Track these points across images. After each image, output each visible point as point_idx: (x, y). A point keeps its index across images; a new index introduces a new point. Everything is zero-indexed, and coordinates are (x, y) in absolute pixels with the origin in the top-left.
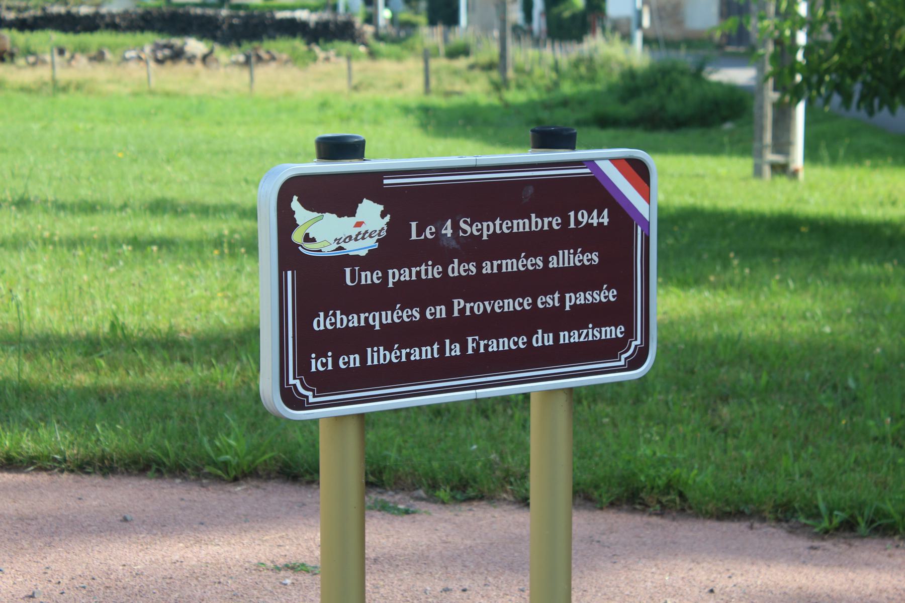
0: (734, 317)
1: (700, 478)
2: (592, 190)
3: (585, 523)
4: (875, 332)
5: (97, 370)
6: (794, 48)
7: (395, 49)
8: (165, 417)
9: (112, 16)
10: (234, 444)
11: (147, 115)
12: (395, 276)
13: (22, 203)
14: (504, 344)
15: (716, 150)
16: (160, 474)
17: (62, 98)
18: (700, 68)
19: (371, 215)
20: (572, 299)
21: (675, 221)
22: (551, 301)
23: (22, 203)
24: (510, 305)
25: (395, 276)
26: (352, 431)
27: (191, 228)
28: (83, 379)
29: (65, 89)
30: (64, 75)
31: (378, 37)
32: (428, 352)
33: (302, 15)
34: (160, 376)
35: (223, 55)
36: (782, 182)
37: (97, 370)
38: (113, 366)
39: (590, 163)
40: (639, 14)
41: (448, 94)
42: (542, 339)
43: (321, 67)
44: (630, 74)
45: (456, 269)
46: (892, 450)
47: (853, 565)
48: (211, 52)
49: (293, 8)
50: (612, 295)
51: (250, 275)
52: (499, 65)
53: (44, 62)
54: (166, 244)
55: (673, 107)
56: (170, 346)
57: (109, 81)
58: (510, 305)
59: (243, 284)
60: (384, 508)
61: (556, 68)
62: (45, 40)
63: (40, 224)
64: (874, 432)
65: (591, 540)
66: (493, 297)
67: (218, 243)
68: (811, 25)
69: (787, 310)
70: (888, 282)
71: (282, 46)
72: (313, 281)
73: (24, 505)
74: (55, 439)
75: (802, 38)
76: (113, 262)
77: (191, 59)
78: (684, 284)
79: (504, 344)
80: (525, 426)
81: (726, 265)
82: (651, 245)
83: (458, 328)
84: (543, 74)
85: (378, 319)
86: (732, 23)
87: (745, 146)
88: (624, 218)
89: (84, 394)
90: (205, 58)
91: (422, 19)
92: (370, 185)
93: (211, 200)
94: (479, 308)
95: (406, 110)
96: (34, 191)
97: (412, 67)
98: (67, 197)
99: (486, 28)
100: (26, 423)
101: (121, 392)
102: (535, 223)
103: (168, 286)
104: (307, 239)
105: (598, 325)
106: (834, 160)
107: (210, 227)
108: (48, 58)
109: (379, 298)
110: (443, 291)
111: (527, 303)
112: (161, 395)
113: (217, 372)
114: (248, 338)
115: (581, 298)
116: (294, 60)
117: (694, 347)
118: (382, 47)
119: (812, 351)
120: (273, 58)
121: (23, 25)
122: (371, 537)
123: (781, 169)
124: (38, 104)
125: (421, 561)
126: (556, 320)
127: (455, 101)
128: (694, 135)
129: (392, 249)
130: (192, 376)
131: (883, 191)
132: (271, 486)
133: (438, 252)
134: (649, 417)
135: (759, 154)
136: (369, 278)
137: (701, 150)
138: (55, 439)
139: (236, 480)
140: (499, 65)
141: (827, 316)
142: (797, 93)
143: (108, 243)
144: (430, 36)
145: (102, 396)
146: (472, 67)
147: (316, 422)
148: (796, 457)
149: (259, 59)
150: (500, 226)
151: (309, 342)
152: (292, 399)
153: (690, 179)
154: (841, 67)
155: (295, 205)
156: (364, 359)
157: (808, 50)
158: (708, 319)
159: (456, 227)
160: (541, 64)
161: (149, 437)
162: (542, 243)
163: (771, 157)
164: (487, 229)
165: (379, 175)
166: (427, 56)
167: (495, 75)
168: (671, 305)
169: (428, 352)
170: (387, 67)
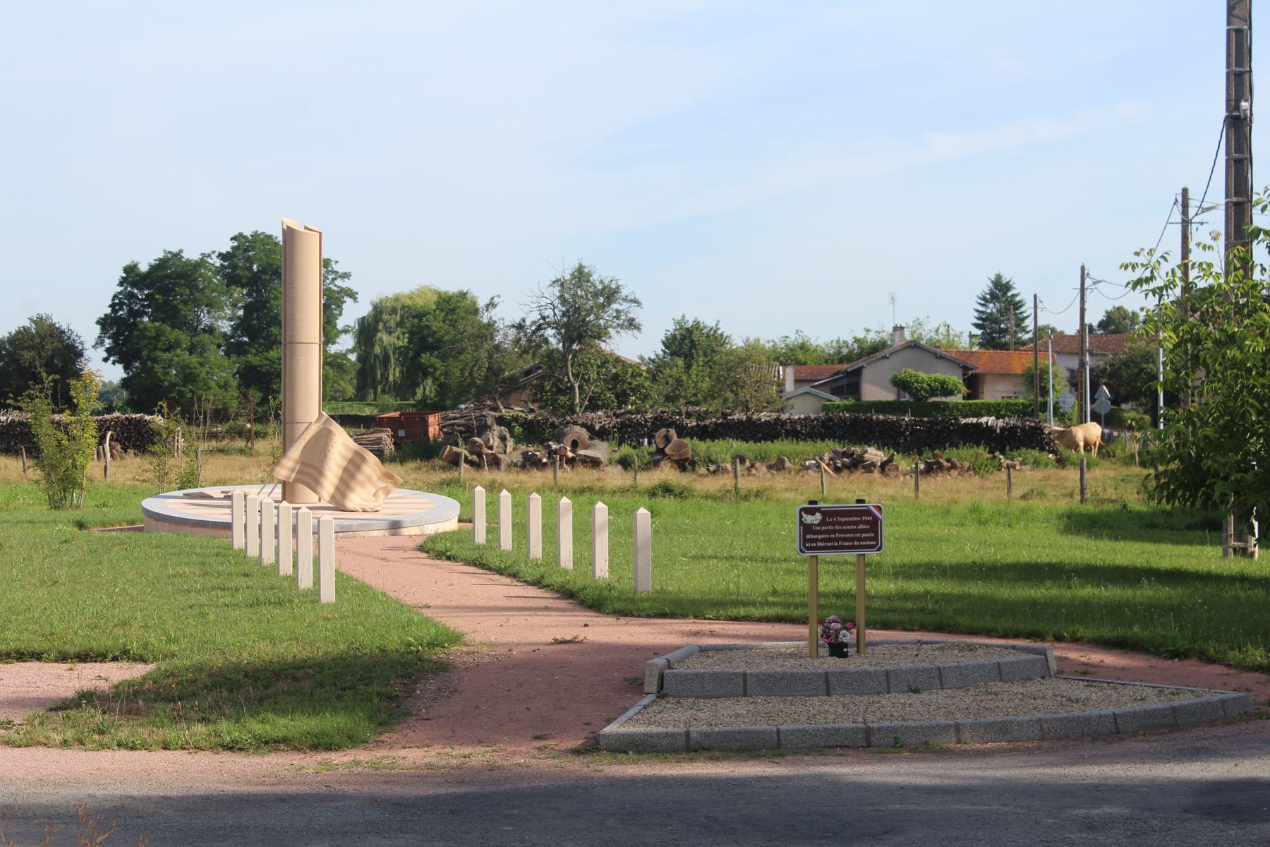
9: (793, 422)
29: (746, 498)
30: (746, 483)
35: (903, 463)
42: (856, 543)
48: (890, 460)
53: (725, 471)
57: (787, 490)
62: (723, 448)
71: (965, 454)
72: (806, 528)
77: (869, 468)
83: (837, 540)
90: (883, 465)
92: (818, 510)
102: (854, 519)
108: (729, 466)
109: (820, 532)
110: (834, 532)
116: (975, 469)
120: (954, 467)
121: (704, 433)
123: (1244, 552)
124: (724, 509)
126: (859, 539)
133: (833, 524)
151: (805, 540)
162: (857, 523)
163: (1233, 543)
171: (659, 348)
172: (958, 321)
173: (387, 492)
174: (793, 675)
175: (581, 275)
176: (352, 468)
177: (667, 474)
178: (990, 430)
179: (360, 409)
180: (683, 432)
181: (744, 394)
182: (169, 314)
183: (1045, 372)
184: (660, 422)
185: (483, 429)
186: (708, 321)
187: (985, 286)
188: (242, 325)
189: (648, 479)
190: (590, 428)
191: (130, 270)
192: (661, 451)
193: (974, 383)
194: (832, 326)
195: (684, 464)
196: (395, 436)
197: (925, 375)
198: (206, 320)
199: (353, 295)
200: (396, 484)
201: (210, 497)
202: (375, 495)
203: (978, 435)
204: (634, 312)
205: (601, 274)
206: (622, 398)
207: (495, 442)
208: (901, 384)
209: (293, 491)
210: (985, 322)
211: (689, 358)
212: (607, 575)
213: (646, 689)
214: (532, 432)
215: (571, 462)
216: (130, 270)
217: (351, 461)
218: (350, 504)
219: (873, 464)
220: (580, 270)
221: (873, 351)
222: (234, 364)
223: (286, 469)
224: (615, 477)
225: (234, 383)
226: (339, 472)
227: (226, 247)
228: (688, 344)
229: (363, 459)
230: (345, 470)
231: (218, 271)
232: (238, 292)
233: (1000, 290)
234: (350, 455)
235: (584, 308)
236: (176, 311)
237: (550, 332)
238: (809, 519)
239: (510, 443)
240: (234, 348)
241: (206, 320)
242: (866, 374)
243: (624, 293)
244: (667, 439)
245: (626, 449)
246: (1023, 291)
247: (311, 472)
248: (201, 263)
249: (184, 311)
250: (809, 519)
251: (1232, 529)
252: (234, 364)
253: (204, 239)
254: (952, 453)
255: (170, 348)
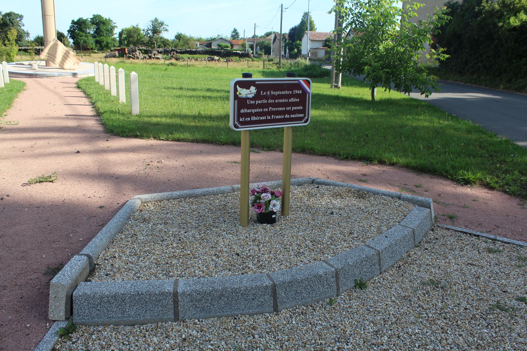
0: (326, 116)
1: (317, 147)
2: (299, 86)
3: (294, 156)
4: (354, 120)
5: (196, 122)
6: (340, 61)
7: (258, 59)
8: (209, 132)
10: (223, 137)
11: (206, 71)
12: (257, 102)
13: (181, 89)
14: (279, 117)
15: (323, 82)
16: (208, 143)
17: (189, 68)
18: (321, 66)
19: (253, 89)
20: (293, 108)
21: (315, 96)
22: (289, 108)
23: (181, 89)
24: (281, 109)
25: (257, 102)
26: (248, 134)
27: (215, 94)
28: (193, 124)
29: (189, 66)
30: (189, 63)
31: (254, 57)
32: (264, 118)
33: (238, 52)
34: (208, 124)
35: (222, 60)
36: (336, 89)
37: (196, 122)
38: (199, 122)
39: (298, 80)
40: (308, 53)
41: (268, 69)
42: (287, 116)
43: (242, 63)
44: (306, 66)
45: (270, 101)
46: (356, 143)
47: (347, 166)
49: (237, 50)
50: (302, 108)
51: (227, 104)
52: (279, 63)
54: (210, 97)
55: (315, 73)
56: (210, 118)
58: (281, 109)
59: (225, 106)
60: (253, 151)
61: (291, 64)
63: (184, 93)
64: (353, 140)
65: (295, 159)
66: (277, 107)
67: (220, 97)
68: (344, 57)
69: (337, 115)
70: (357, 110)
71: (234, 58)
72: (241, 102)
73: (181, 148)
74: (187, 135)
75: (342, 59)
76: (199, 101)
77: (215, 60)
78: (316, 109)
79: (279, 117)
80: (283, 136)
81: (324, 105)
82: (309, 100)
83: (270, 113)
84: (288, 65)
85: (254, 111)
86: (327, 56)
87: (329, 82)
88: (305, 92)
89: (193, 127)
90: (218, 60)
91: (263, 53)
92: (253, 83)
93: (219, 89)
94: (274, 109)
95: (259, 72)
96: (183, 86)
97: (261, 63)
98: (190, 87)
99: (276, 56)
100: (182, 132)
101: (200, 126)
102: (287, 92)
103: (210, 106)
104: (240, 94)
105: (299, 114)
106: (347, 85)
107: (219, 94)
110: (267, 105)
111: (284, 108)
112: (208, 128)
113: (220, 123)
114: (227, 117)
115: (295, 108)
117: (317, 121)
118: (255, 59)
119: (341, 123)
121: (181, 53)
122: (251, 157)
123: (336, 87)
125: (260, 162)
126: (290, 112)
127: (270, 70)
128: (319, 79)
129: (257, 97)
130: (215, 124)
131: (357, 92)
132: (230, 146)
133: (266, 97)
134: (308, 135)
135: (332, 84)
136: (252, 102)
137: (320, 82)
138: (187, 135)
139: (223, 145)
140: (279, 63)
141: (344, 116)
142: (340, 71)
143: (198, 97)
144: (265, 57)
145: (196, 127)
146: (273, 63)
147: (240, 131)
148: (337, 144)
149: (229, 61)
150: (279, 93)
151: (240, 115)
152: (236, 126)
153: (318, 88)
154: (349, 66)
155: (238, 87)
156: (251, 119)
157: (343, 62)
158: (320, 116)
159: (270, 92)
160: (287, 63)
161: (206, 136)
162: (288, 97)
163: (334, 84)
164: (276, 93)
165: (255, 81)
166: (264, 61)
167: (278, 65)
168: (313, 113)
169: (264, 118)
170: (256, 63)
171: (174, 38)
172: (227, 35)
173: (78, 64)
174: (235, 291)
175: (156, 20)
176: (66, 56)
177: (173, 61)
178: (239, 53)
179: (431, 121)
180: (177, 52)
181: (190, 46)
182: (81, 30)
183: (245, 44)
184: (172, 50)
185: (136, 51)
186: (183, 33)
187: (232, 30)
188: (95, 32)
189: (168, 62)
190: (158, 51)
191: (73, 21)
192: (172, 56)
193: (232, 46)
194: (206, 35)
195: (177, 59)
196: (119, 53)
197: (223, 44)
198: (88, 31)
199: (116, 27)
200: (80, 61)
201: (23, 64)
202: (74, 64)
203: (236, 54)
204: (167, 28)
205: (160, 20)
206: (165, 45)
207: (138, 54)
208: (219, 46)
209: (49, 63)
210: (232, 36)
211: (179, 39)
212: (125, 101)
213: (51, 316)
214: (146, 52)
215: (153, 58)
216: (73, 21)
217: (65, 54)
218: (65, 67)
220: (156, 19)
221: (214, 39)
222: (94, 39)
223: (44, 55)
224: (162, 61)
225: (94, 43)
226: (61, 57)
227: (92, 17)
228: (179, 37)
229: (69, 53)
230: (63, 56)
231: (91, 22)
232: (94, 26)
233: (235, 31)
234: (65, 52)
235: (156, 27)
236: (82, 29)
237: (150, 32)
238: (243, 93)
239: (141, 54)
240: (94, 37)
241: (88, 31)
242: (213, 44)
243: (165, 24)
244: (174, 54)
245: (165, 56)
246: (238, 31)
247: (52, 57)
248: (86, 20)
249: (84, 29)
250: (243, 93)
251: (334, 80)
252: (94, 39)
253: (87, 16)
254: (231, 58)
255: (81, 36)
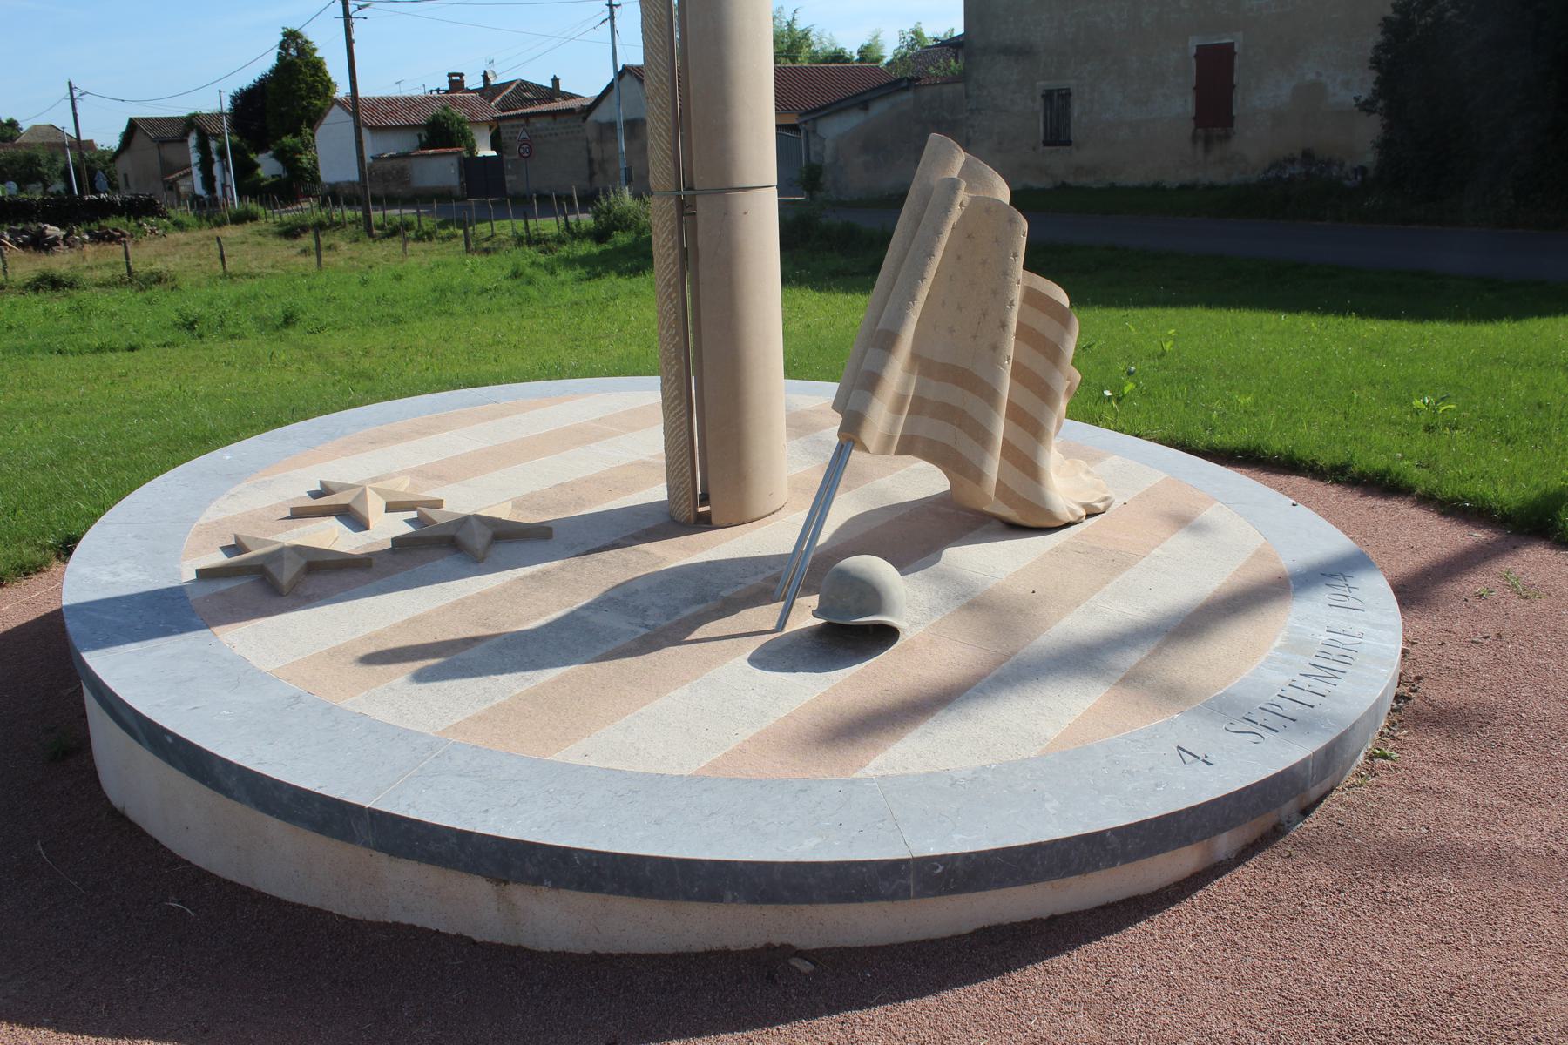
219: (57, 238)
